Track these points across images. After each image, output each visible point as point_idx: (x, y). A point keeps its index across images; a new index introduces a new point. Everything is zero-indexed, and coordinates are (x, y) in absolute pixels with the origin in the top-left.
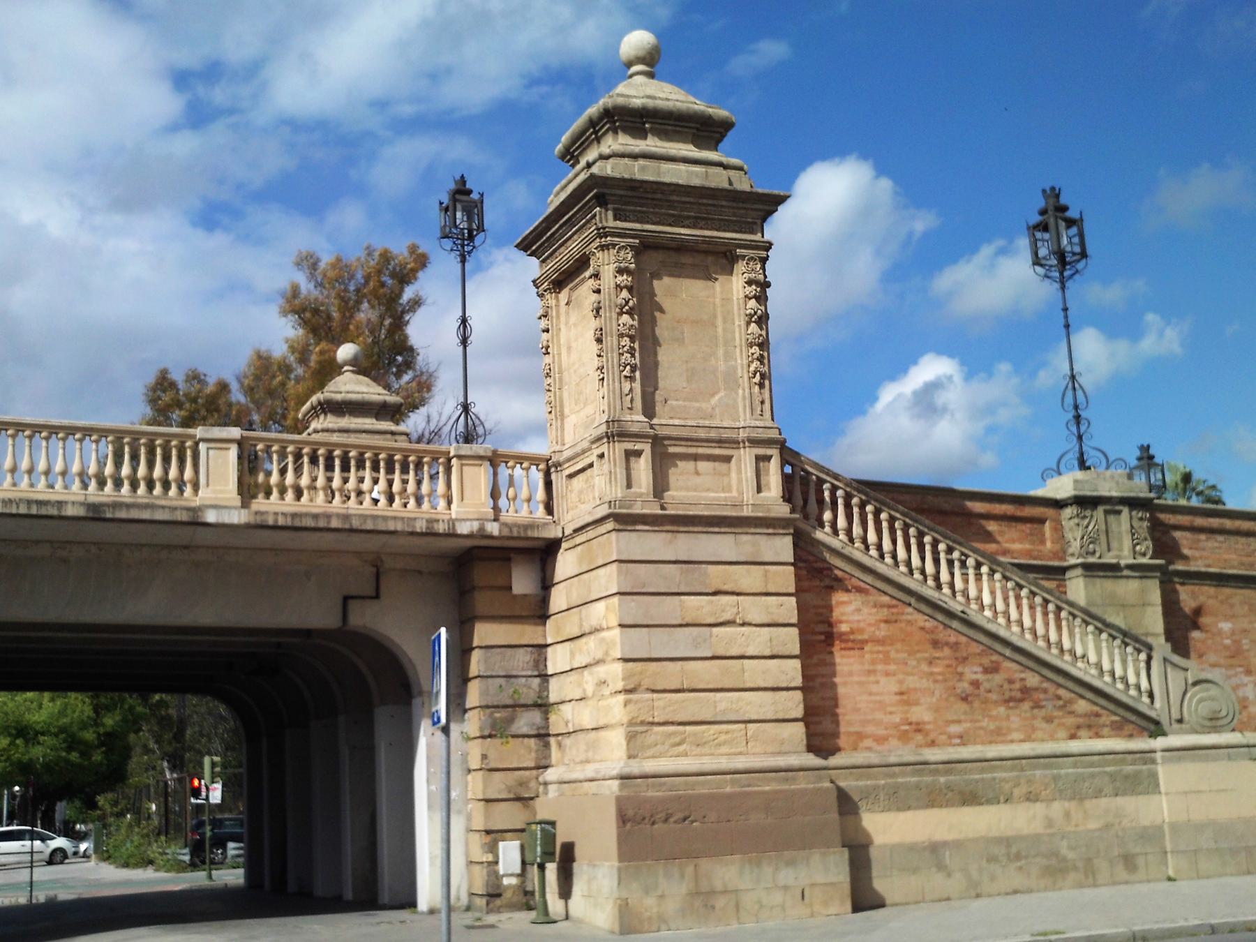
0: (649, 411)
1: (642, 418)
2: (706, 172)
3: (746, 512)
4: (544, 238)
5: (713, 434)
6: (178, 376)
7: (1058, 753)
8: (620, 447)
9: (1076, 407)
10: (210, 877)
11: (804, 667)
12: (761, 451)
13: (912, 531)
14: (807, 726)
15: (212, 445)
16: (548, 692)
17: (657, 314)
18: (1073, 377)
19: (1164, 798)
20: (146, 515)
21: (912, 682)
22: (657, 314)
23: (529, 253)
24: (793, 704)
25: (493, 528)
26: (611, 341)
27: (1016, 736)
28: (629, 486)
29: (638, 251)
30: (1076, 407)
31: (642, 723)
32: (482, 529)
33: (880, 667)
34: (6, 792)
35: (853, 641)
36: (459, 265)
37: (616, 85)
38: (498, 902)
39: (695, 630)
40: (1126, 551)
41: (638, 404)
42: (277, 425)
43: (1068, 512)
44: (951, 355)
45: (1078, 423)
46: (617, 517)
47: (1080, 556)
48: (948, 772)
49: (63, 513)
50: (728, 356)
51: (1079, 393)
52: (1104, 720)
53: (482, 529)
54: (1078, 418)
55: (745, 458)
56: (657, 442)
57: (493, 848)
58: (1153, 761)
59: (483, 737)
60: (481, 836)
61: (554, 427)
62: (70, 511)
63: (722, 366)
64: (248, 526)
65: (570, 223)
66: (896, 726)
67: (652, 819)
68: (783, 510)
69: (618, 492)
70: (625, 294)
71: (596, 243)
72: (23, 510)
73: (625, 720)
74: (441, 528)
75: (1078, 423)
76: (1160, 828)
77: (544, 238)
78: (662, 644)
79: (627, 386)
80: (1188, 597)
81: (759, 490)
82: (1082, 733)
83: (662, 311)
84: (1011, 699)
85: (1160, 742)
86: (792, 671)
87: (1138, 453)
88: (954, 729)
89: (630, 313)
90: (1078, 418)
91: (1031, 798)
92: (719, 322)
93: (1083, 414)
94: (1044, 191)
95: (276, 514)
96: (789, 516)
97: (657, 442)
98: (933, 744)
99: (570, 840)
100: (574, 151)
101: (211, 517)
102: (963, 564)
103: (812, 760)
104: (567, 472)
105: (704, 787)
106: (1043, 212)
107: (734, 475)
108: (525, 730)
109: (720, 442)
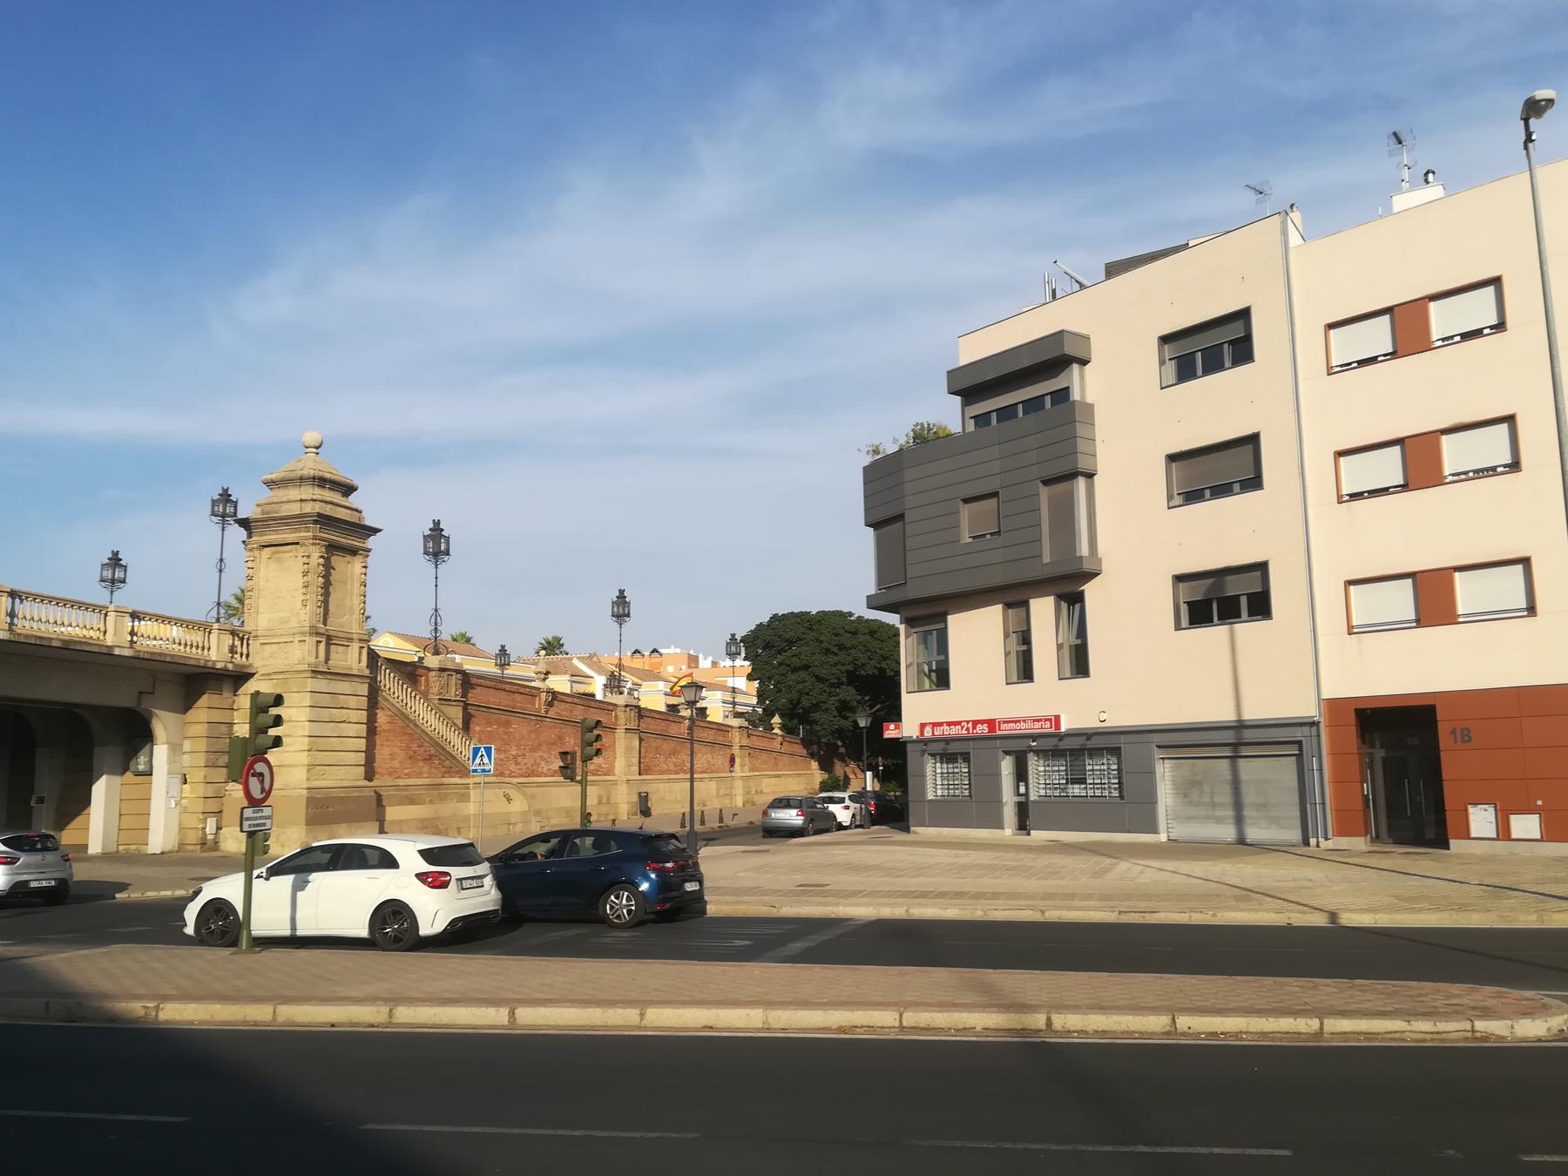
0: (325, 624)
1: (322, 626)
2: (47, 1004)
3: (355, 672)
4: (958, 1144)
5: (345, 635)
6: (446, 558)
7: (1534, 180)
8: (315, 639)
9: (436, 624)
10: (642, 1015)
11: (366, 756)
12: (361, 645)
13: (400, 682)
14: (367, 741)
15: (119, 614)
16: (1366, 709)
17: (332, 571)
18: (436, 610)
19: (472, 804)
20: (88, 648)
21: (396, 750)
22: (332, 571)
23: (1200, 371)
24: (361, 758)
25: (230, 666)
26: (312, 589)
27: (425, 775)
28: (317, 658)
29: (327, 547)
30: (436, 624)
31: (312, 765)
32: (225, 666)
33: (385, 743)
34: (697, 1135)
35: (1382, 994)
36: (221, 532)
37: (501, 884)
38: (205, 847)
39: (332, 724)
40: (453, 694)
41: (322, 619)
42: (783, 654)
43: (433, 674)
44: (102, 775)
45: (436, 632)
46: (313, 671)
47: (437, 695)
48: (406, 790)
49: (1372, 915)
50: (351, 600)
51: (439, 618)
52: (453, 770)
53: (225, 666)
54: (436, 629)
55: (355, 646)
56: (329, 638)
57: (205, 821)
58: (469, 788)
59: (205, 767)
60: (568, 812)
61: (1308, 1000)
62: (55, 644)
63: (348, 604)
64: (132, 657)
65: (287, 524)
66: (387, 769)
67: (835, 650)
68: (367, 672)
69: (313, 660)
70: (321, 568)
71: (311, 541)
72: (33, 642)
73: (306, 763)
74: (210, 664)
75: (436, 632)
76: (469, 816)
77: (958, 1144)
78: (327, 729)
79: (318, 610)
80: (471, 710)
81: (1159, 747)
82: (446, 775)
83: (334, 569)
84: (425, 759)
85: (471, 781)
86: (363, 716)
87: (730, 637)
88: (406, 771)
89: (322, 577)
90: (436, 629)
91: (431, 802)
92: (349, 582)
93: (439, 628)
94: (434, 520)
95: (144, 652)
96: (861, 610)
97: (329, 638)
98: (399, 777)
99: (862, 470)
100: (1087, 984)
101: (117, 652)
102: (415, 697)
103: (366, 783)
104: (262, 641)
105: (336, 793)
106: (703, 710)
107: (350, 654)
108: (222, 764)
109: (804, 892)
